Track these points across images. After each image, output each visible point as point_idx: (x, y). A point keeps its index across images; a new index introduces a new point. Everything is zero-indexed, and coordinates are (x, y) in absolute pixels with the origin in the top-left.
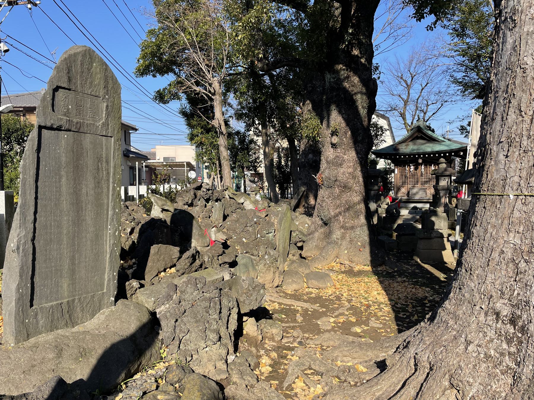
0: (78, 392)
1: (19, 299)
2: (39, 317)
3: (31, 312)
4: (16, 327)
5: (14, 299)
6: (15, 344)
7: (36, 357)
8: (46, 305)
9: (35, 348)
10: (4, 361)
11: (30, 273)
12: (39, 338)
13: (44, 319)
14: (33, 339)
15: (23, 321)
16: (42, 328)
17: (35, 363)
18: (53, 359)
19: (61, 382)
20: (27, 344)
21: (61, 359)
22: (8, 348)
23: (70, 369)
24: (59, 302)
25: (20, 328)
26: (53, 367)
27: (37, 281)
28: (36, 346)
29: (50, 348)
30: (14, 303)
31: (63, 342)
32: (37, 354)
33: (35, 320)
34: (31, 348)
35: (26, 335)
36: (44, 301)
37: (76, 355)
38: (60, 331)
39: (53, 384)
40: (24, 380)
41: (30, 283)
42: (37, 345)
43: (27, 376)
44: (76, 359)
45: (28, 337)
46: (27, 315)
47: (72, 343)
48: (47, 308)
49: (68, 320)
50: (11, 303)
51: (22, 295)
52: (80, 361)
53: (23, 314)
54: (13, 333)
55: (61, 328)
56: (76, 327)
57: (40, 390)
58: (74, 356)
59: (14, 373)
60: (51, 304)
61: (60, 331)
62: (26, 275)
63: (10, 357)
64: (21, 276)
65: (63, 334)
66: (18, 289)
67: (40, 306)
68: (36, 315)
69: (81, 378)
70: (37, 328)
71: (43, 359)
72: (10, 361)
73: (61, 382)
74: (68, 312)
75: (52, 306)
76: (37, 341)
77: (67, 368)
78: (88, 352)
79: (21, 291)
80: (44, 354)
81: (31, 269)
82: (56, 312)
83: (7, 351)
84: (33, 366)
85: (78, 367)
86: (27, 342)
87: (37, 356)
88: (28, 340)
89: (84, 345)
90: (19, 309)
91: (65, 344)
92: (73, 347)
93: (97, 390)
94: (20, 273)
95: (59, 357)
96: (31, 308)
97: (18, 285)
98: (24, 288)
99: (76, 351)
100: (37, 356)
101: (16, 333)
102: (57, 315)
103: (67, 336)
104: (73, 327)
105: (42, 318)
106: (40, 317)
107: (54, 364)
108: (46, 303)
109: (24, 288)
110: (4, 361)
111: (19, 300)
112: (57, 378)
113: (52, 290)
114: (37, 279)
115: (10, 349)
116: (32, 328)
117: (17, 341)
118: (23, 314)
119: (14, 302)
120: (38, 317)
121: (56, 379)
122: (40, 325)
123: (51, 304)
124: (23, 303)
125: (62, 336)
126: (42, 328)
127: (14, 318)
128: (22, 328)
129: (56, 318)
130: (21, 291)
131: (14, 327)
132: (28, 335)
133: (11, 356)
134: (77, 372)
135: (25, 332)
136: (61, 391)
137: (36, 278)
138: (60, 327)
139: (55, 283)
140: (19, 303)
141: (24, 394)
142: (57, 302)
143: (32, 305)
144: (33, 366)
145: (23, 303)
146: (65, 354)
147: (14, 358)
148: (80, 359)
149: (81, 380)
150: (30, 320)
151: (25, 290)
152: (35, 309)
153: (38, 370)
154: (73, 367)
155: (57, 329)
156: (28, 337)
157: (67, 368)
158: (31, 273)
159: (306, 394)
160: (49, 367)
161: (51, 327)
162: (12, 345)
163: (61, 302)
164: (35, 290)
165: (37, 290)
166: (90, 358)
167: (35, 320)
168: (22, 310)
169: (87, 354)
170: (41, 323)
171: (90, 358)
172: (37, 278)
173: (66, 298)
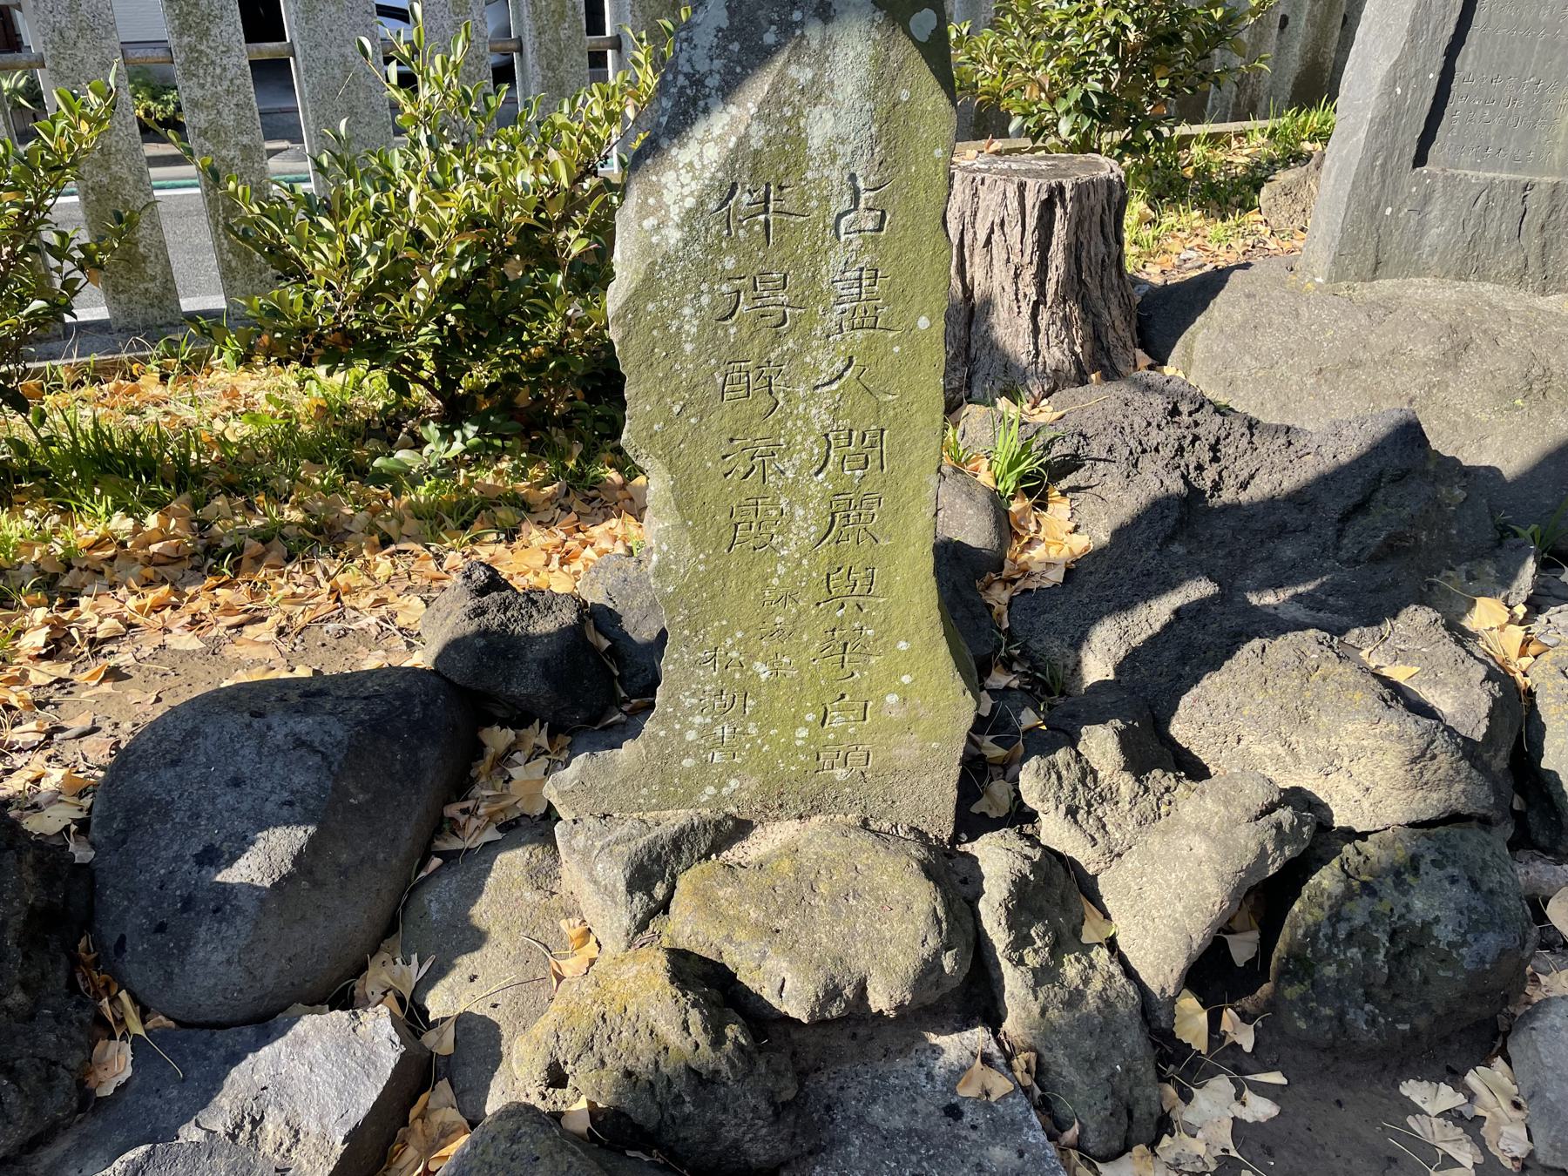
0: (1460, 494)
1: (1384, 121)
2: (1435, 211)
3: (1411, 182)
4: (1348, 220)
5: (1369, 116)
6: (1329, 279)
7: (1373, 338)
8: (1470, 173)
9: (1381, 312)
10: (1277, 319)
11: (1450, 29)
12: (1411, 284)
13: (1447, 223)
14: (1388, 282)
15: (1377, 206)
16: (1432, 254)
17: (1361, 355)
18: (1425, 364)
19: (1409, 435)
20: (1364, 291)
21: (1450, 374)
22: (1303, 286)
23: (1468, 418)
24: (1524, 178)
25: (1360, 230)
26: (1415, 391)
27: (1467, 68)
28: (1388, 306)
29: (1427, 325)
30: (1362, 135)
31: (1481, 322)
32: (1379, 331)
33: (1415, 217)
34: (1369, 308)
35: (1372, 260)
36: (1467, 158)
37: (1509, 381)
38: (1489, 286)
39: (1379, 428)
40: (1310, 394)
41: (1439, 67)
42: (1392, 304)
43: (1325, 388)
44: (1504, 394)
45: (1377, 269)
46: (1395, 192)
47: (1512, 338)
48: (1470, 185)
49: (1530, 261)
50: (1355, 132)
51: (1398, 108)
52: (1517, 408)
53: (1384, 181)
54: (1333, 238)
55: (1497, 281)
56: (1552, 298)
57: (1338, 435)
58: (1501, 382)
59: (1291, 362)
60: (1490, 175)
61: (1487, 288)
62: (1434, 33)
63: (1298, 315)
64: (1414, 33)
65: (1495, 299)
66: (1392, 79)
67: (1450, 171)
68: (1427, 199)
69: (1497, 464)
70: (1415, 250)
71: (1392, 352)
72: (1292, 325)
73: (1409, 435)
74: (1543, 227)
75: (1490, 185)
76: (1400, 293)
77: (1458, 413)
78: (1559, 391)
79: (1399, 91)
80: (1401, 337)
81: (1456, 15)
82: (1498, 213)
83: (1296, 292)
84: (1354, 364)
85: (1501, 424)
86: (1367, 285)
87: (1379, 337)
88: (1373, 279)
89: (1553, 361)
90: (1375, 159)
91: (1485, 332)
92: (1509, 351)
93: (1534, 527)
94: (1414, 20)
95: (1446, 367)
96: (1414, 167)
97: (1395, 64)
98: (1413, 85)
99: (1514, 366)
100: (1379, 337)
101: (1342, 244)
102: (1500, 223)
103: (1506, 311)
104: (1544, 292)
105: (1442, 220)
106: (1436, 212)
107: (1420, 380)
108: (1474, 166)
109: (1413, 85)
110: (1277, 319)
111: (1385, 123)
112: (1403, 414)
113: (1511, 121)
114: (1466, 62)
115: (1307, 291)
116: (1399, 245)
117: (1338, 273)
118: (1383, 187)
119: (1366, 127)
120: (1428, 209)
121: (1397, 416)
122: (1426, 241)
123: (1490, 175)
124: (1394, 141)
125: (1490, 304)
126: (1432, 254)
127: (1349, 187)
128: (1364, 232)
129: (1490, 234)
130: (1399, 91)
131: (1340, 221)
132: (1378, 263)
133: (1304, 311)
134: (1489, 441)
135: (1371, 251)
136: (1396, 461)
137: (1465, 57)
138: (1493, 273)
139: (1529, 94)
140: (1381, 139)
141: (1288, 429)
142: (1513, 176)
143: (1420, 159)
144: (1354, 364)
145: (1394, 141)
146: (1473, 364)
147: (1309, 318)
148: (1518, 402)
149: (1493, 472)
150: (1399, 210)
151: (1414, 90)
152: (1429, 175)
153: (1366, 381)
154: (1484, 417)
155: (1483, 278)
156: (1376, 269)
157: (1458, 413)
158: (1452, 31)
159: (525, 543)
160: (1402, 384)
161: (1464, 261)
162: (1319, 280)
163: (1528, 178)
164: (1450, 105)
165: (1455, 103)
166: (1557, 412)
167: (1415, 217)
168: (1383, 165)
169: (1549, 392)
170: (1434, 234)
171: (1557, 412)
172: (1471, 57)
173: (1552, 172)
